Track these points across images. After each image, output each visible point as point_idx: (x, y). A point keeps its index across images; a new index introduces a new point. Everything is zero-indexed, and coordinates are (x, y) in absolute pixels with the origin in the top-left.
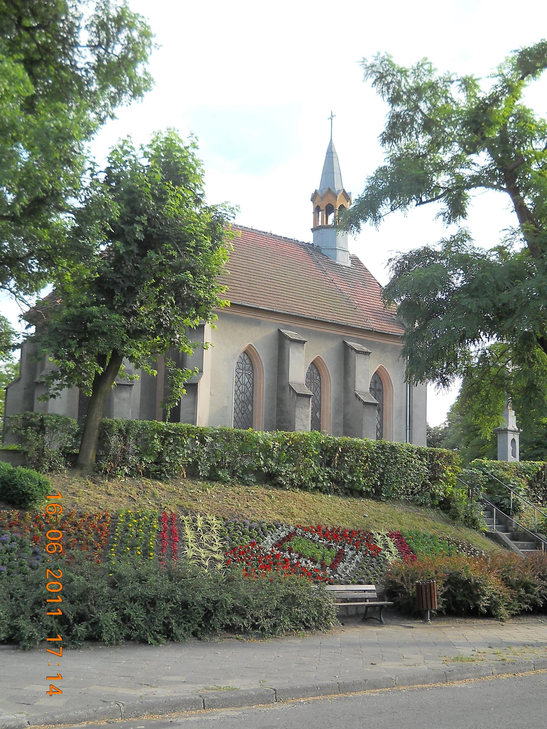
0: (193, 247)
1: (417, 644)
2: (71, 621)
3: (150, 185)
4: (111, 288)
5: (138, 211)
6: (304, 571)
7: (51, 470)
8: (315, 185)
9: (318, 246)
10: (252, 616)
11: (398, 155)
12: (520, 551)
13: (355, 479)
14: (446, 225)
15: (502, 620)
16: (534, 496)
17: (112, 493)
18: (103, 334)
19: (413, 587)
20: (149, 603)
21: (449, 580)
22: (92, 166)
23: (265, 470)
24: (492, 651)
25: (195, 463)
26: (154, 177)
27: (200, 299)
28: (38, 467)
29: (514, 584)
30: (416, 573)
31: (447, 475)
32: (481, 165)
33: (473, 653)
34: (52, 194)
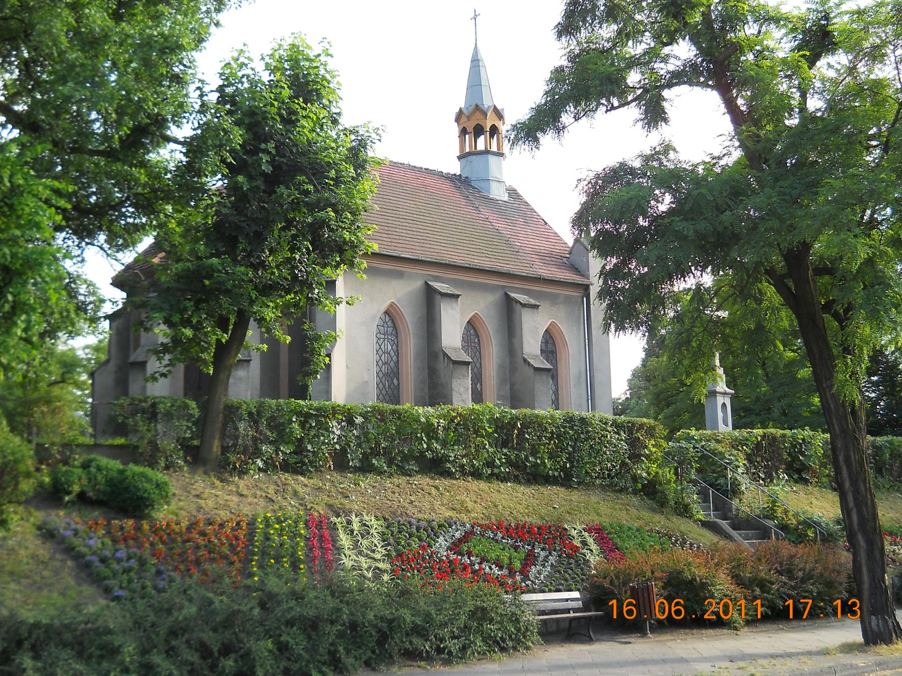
0: (332, 179)
1: (643, 662)
2: (216, 654)
3: (276, 103)
4: (234, 234)
5: (263, 137)
6: (487, 578)
7: (167, 468)
8: (459, 101)
9: (467, 178)
10: (435, 637)
11: (577, 51)
12: (746, 544)
13: (539, 461)
14: (646, 133)
15: (736, 629)
16: (754, 474)
17: (245, 492)
18: (227, 292)
19: (626, 592)
20: (310, 626)
21: (669, 581)
22: (200, 85)
23: (429, 455)
24: (735, 665)
25: (344, 451)
26: (281, 93)
27: (345, 242)
28: (152, 464)
29: (747, 583)
30: (628, 574)
31: (650, 450)
32: (683, 58)
33: (713, 669)
34: (157, 121)
